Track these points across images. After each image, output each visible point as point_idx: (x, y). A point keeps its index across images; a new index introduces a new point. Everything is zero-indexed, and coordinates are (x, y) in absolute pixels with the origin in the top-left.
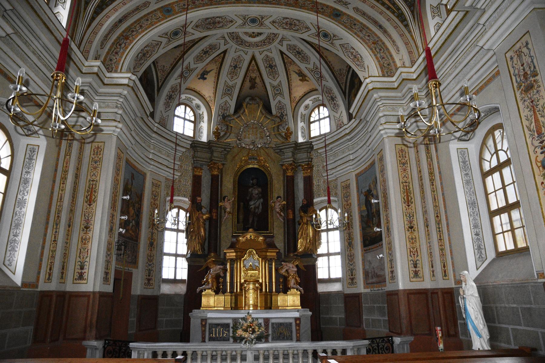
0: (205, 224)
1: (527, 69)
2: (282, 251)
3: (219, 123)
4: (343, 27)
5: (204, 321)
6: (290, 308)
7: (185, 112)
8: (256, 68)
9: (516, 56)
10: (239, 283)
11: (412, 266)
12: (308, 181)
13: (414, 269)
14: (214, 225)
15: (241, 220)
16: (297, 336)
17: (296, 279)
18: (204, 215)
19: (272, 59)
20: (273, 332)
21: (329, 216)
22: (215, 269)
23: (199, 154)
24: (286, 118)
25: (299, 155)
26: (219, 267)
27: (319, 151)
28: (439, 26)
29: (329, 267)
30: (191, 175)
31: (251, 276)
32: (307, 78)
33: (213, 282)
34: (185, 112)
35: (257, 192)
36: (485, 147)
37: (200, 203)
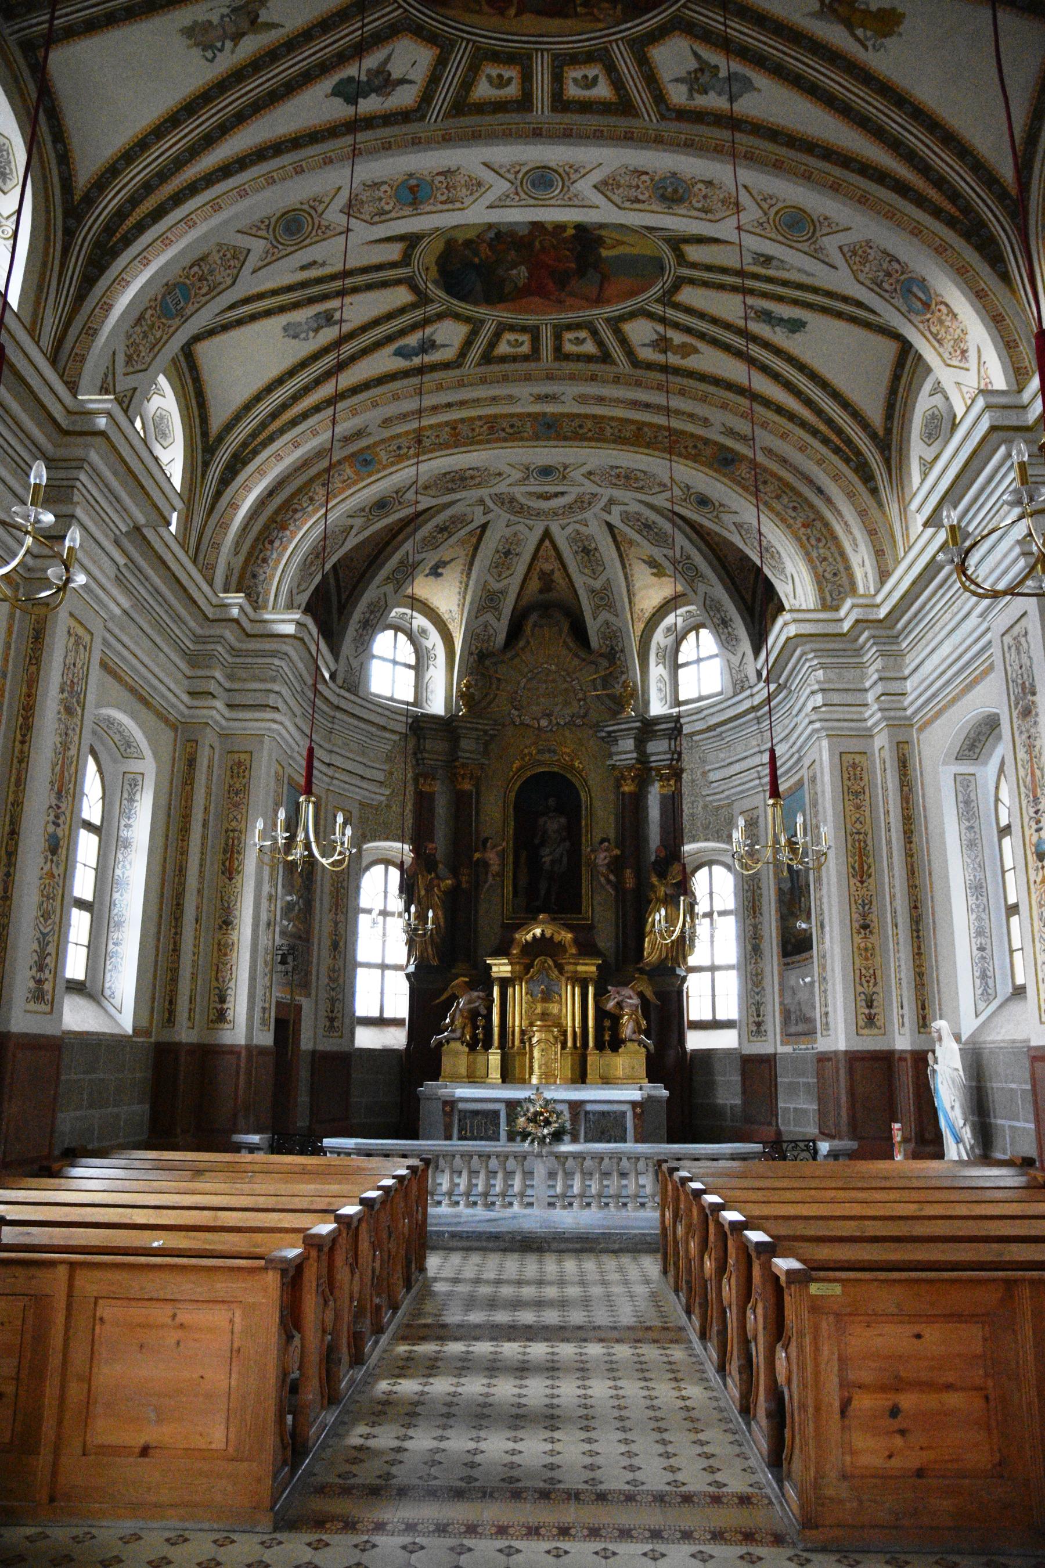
4: (741, 491)
8: (553, 553)
11: (864, 1004)
12: (673, 806)
13: (867, 1011)
17: (638, 1023)
19: (591, 538)
21: (715, 888)
29: (713, 996)
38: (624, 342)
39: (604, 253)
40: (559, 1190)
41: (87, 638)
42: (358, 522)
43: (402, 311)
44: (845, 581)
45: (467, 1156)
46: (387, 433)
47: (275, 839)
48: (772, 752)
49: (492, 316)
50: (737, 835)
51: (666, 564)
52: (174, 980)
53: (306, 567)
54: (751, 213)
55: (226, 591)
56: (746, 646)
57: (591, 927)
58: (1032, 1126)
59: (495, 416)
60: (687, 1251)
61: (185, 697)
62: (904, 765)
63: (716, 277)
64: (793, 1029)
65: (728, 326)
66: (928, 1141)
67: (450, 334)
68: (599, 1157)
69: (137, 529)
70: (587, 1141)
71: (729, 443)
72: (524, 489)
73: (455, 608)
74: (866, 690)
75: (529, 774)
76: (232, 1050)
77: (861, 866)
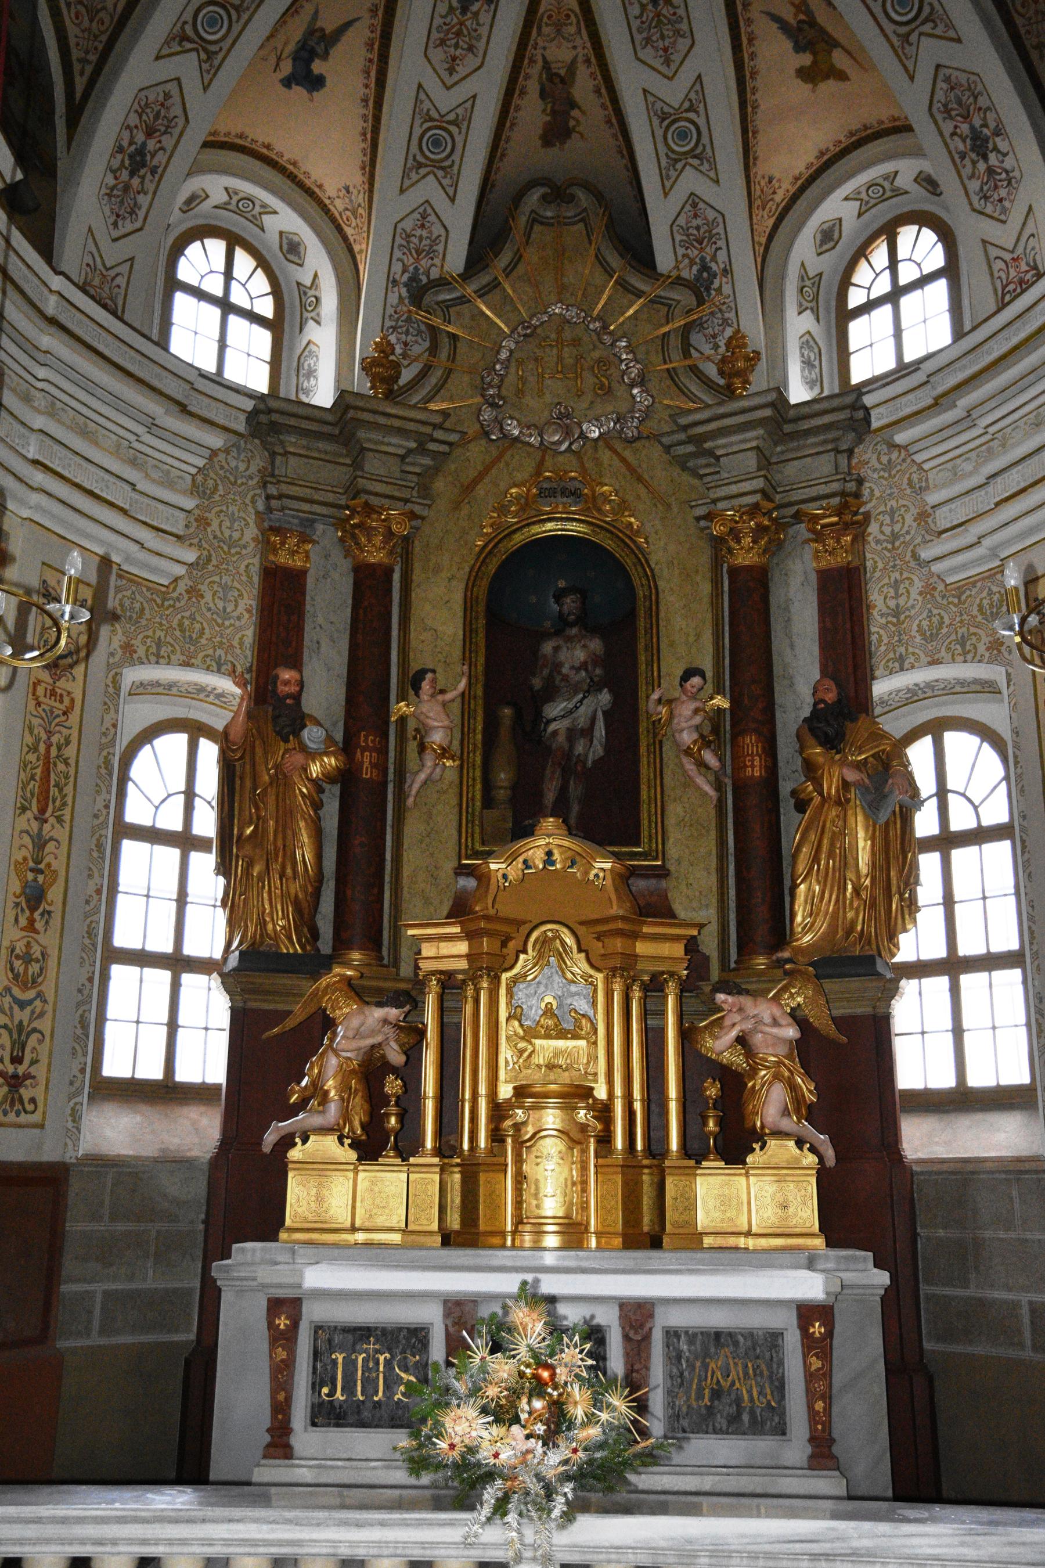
0: (317, 806)
2: (710, 945)
3: (394, 322)
5: (285, 1307)
6: (763, 1242)
7: (228, 274)
10: (483, 1103)
12: (843, 597)
14: (365, 808)
15: (502, 794)
16: (813, 1416)
17: (793, 1087)
18: (313, 756)
20: (677, 1381)
22: (361, 1027)
23: (293, 467)
24: (727, 289)
25: (791, 470)
26: (379, 1013)
27: (900, 438)
30: (255, 570)
31: (551, 1067)
32: (839, 59)
33: (344, 1088)
34: (228, 274)
35: (580, 655)
37: (297, 697)
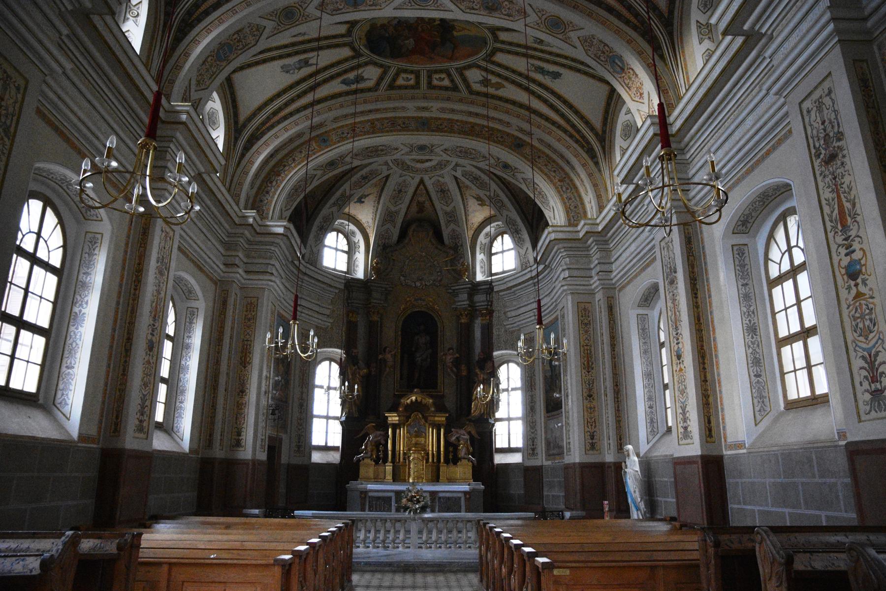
1: (829, 129)
9: (815, 109)
12: (487, 331)
17: (468, 449)
21: (510, 375)
28: (709, 55)
36: (773, 241)
38: (465, 80)
39: (455, 33)
40: (424, 538)
41: (171, 234)
42: (319, 173)
43: (346, 60)
44: (581, 210)
45: (374, 520)
46: (335, 126)
47: (277, 343)
48: (539, 301)
49: (394, 64)
50: (520, 344)
51: (486, 199)
52: (213, 423)
53: (291, 196)
54: (533, 18)
55: (246, 209)
56: (528, 244)
57: (443, 396)
58: (674, 500)
59: (395, 118)
60: (493, 565)
61: (222, 267)
62: (611, 309)
63: (515, 49)
64: (551, 452)
65: (520, 74)
66: (622, 510)
67: (372, 73)
68: (447, 520)
69: (200, 174)
70: (439, 512)
71: (520, 135)
72: (410, 157)
73: (370, 221)
74: (591, 269)
75: (409, 312)
76: (244, 463)
77: (588, 363)
